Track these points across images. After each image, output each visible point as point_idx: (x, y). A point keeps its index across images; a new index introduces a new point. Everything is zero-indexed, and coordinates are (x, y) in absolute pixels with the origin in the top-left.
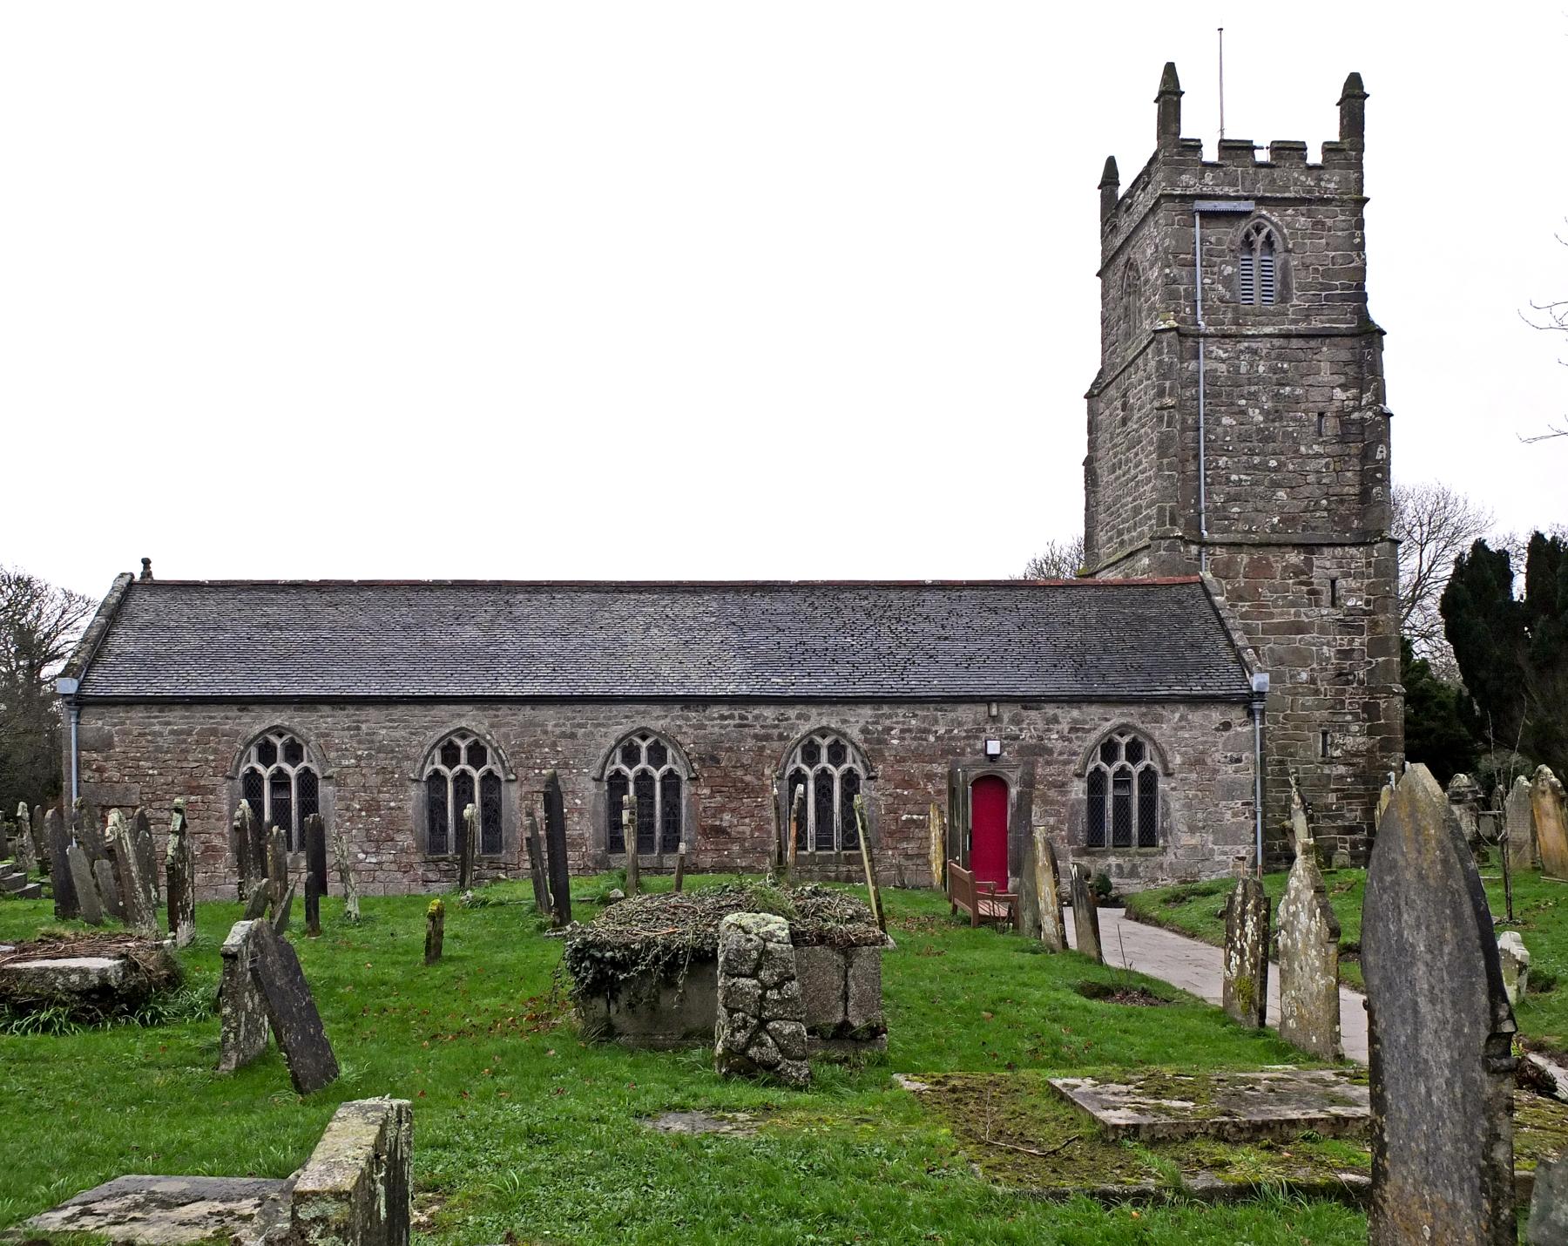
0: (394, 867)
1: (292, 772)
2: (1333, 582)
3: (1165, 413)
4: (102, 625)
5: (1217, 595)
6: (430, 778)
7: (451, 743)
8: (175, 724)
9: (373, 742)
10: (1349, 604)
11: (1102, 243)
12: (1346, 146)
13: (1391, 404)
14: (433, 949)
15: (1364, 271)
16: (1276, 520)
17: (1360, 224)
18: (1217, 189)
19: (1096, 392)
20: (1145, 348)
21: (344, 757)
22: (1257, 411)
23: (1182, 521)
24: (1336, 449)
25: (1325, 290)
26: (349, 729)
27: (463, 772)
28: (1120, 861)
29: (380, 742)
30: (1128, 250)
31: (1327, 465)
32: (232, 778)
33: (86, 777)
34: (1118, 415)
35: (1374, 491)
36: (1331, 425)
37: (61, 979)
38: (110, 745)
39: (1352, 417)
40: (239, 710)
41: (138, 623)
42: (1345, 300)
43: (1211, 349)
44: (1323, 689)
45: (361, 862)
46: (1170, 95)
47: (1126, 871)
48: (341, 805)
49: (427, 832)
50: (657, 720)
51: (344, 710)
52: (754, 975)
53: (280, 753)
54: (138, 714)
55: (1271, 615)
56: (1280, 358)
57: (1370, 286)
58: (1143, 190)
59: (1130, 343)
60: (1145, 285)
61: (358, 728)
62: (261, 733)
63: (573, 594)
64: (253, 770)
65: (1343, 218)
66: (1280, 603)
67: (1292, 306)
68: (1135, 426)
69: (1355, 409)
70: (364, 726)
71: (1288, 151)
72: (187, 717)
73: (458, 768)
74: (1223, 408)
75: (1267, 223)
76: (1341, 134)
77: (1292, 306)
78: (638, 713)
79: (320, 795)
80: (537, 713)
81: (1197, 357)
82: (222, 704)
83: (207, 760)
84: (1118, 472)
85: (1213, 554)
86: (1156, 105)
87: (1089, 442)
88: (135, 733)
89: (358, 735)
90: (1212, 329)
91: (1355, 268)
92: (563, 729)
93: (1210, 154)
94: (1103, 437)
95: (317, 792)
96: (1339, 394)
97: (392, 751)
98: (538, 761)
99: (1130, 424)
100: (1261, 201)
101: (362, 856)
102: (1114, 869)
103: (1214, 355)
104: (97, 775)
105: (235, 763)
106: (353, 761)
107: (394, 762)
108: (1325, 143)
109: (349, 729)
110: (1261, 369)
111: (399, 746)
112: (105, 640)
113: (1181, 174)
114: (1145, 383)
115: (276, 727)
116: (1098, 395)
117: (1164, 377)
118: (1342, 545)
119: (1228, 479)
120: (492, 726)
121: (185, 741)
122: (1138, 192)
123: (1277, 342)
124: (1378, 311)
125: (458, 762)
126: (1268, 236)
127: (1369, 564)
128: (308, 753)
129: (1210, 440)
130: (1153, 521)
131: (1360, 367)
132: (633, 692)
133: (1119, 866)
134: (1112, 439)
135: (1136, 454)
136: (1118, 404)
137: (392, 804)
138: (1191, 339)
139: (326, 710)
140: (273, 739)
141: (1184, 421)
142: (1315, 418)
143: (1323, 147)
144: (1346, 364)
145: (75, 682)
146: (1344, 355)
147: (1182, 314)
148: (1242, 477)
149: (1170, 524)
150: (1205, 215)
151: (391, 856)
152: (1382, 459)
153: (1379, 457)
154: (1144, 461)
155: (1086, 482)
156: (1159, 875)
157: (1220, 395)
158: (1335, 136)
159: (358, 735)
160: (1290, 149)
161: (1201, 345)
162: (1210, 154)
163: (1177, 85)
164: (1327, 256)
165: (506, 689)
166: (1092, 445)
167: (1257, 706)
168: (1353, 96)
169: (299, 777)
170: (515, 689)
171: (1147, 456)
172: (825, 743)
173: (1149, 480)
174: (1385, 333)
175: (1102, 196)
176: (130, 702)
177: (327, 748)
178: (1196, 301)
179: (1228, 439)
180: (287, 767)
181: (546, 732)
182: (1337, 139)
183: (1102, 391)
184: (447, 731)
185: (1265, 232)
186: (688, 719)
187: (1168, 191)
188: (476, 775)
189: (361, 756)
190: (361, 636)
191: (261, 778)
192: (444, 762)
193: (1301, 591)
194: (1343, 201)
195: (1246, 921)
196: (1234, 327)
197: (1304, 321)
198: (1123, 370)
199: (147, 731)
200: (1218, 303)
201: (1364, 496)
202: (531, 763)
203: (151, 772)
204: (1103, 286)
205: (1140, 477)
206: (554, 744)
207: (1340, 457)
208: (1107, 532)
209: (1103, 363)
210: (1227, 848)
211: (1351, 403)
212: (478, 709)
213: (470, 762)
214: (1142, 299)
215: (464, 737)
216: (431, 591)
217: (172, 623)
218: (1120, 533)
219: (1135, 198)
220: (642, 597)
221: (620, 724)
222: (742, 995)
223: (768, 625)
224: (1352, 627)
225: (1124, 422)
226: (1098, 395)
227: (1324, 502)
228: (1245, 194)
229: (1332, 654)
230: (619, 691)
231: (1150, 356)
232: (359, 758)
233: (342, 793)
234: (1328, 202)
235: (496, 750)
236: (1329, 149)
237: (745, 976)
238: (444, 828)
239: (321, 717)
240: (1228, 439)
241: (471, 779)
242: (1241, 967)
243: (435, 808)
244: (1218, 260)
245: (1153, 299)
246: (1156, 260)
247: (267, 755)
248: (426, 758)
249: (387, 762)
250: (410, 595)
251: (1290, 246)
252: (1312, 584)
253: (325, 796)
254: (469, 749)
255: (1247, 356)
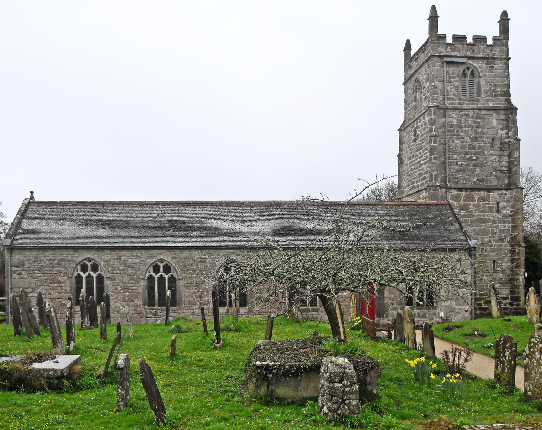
0: (134, 312)
1: (94, 275)
2: (498, 203)
3: (433, 138)
4: (19, 219)
5: (455, 209)
6: (148, 278)
7: (157, 264)
8: (49, 257)
9: (126, 264)
10: (504, 212)
11: (405, 72)
12: (502, 38)
13: (520, 136)
14: (173, 355)
15: (509, 85)
16: (475, 180)
17: (508, 68)
18: (452, 53)
19: (402, 129)
20: (424, 113)
21: (114, 269)
22: (468, 138)
23: (439, 179)
24: (499, 153)
25: (494, 92)
26: (117, 259)
27: (161, 275)
28: (419, 311)
29: (129, 264)
30: (416, 75)
31: (495, 159)
32: (71, 278)
33: (14, 277)
34: (412, 138)
35: (514, 169)
36: (497, 144)
37: (46, 373)
38: (24, 265)
39: (505, 141)
40: (74, 252)
41: (33, 217)
42: (502, 96)
43: (450, 114)
44: (494, 245)
45: (121, 310)
46: (433, 19)
47: (421, 315)
48: (114, 288)
49: (147, 298)
50: (237, 257)
51: (115, 251)
52: (341, 382)
53: (89, 268)
54: (34, 253)
55: (474, 216)
56: (477, 117)
57: (511, 91)
58: (423, 53)
59: (417, 111)
60: (423, 89)
61: (120, 259)
62: (83, 260)
63: (203, 207)
64: (79, 275)
65: (501, 65)
66: (477, 211)
67: (481, 98)
68: (419, 143)
69: (506, 138)
70: (122, 258)
71: (480, 40)
72: (54, 254)
73: (159, 274)
74: (455, 137)
75: (472, 66)
76: (500, 33)
77: (481, 98)
78: (230, 253)
79: (105, 284)
80: (191, 253)
81: (445, 117)
82: (67, 249)
83: (61, 270)
84: (412, 160)
85: (451, 192)
86: (428, 21)
87: (400, 147)
88: (33, 260)
89: (120, 261)
90: (450, 106)
91: (506, 84)
92: (201, 259)
93: (449, 40)
94: (405, 146)
95: (104, 283)
96: (500, 132)
97: (134, 267)
98: (191, 271)
99: (417, 141)
100: (470, 58)
101: (121, 308)
102: (416, 314)
103: (451, 116)
104: (18, 276)
105: (72, 272)
106: (118, 271)
107: (134, 272)
108: (494, 37)
109: (117, 259)
110: (470, 122)
111: (136, 265)
112: (21, 224)
113: (438, 47)
114: (424, 126)
115: (88, 258)
116: (403, 130)
117: (432, 124)
118: (501, 189)
119: (457, 163)
120: (173, 258)
121: (52, 263)
122: (421, 54)
123: (476, 111)
124: (514, 100)
125: (159, 272)
126: (472, 71)
127: (512, 197)
128: (101, 269)
129: (450, 149)
130: (428, 179)
131: (508, 122)
132: (229, 245)
133: (419, 314)
134: (409, 147)
135: (420, 153)
136: (412, 133)
137: (134, 288)
138: (442, 110)
139: (108, 252)
140: (87, 263)
141: (440, 141)
142: (491, 141)
143: (493, 38)
144: (503, 120)
145: (10, 240)
146: (503, 117)
147: (439, 101)
148: (462, 163)
149: (435, 181)
150: (448, 63)
151: (133, 308)
152: (517, 157)
153: (515, 156)
154: (423, 156)
155: (398, 163)
156: (434, 317)
157: (454, 131)
158: (497, 34)
159: (120, 261)
160: (480, 39)
161: (447, 112)
162: (449, 40)
163: (436, 14)
164: (495, 79)
165: (179, 244)
166: (401, 149)
167: (473, 252)
168: (504, 19)
169: (97, 277)
170: (182, 244)
171: (425, 154)
172: (161, 265)
173: (425, 163)
174: (517, 109)
175: (405, 54)
176: (31, 248)
177: (108, 266)
178: (444, 96)
179: (457, 148)
180: (92, 274)
181: (194, 261)
182: (498, 35)
183: (405, 128)
184: (155, 260)
185: (471, 70)
186: (250, 256)
187: (433, 54)
188: (167, 277)
189: (121, 269)
190: (120, 223)
191: (82, 277)
192: (154, 272)
193: (485, 207)
194: (501, 59)
195: (506, 351)
196: (459, 106)
197: (486, 104)
198: (414, 121)
199: (38, 259)
200: (453, 96)
201: (510, 170)
202: (188, 272)
203: (39, 275)
204: (405, 89)
205: (422, 162)
206: (197, 265)
207: (500, 156)
208: (407, 182)
209: (405, 117)
210: (460, 307)
211: (505, 135)
212: (167, 252)
213: (164, 272)
214: (422, 94)
215: (162, 262)
216: (147, 205)
217: (46, 218)
218: (413, 183)
219: (419, 56)
220: (230, 208)
221: (221, 258)
222: (336, 390)
223: (280, 219)
224: (505, 221)
225: (415, 140)
226: (403, 130)
227: (494, 173)
228: (463, 55)
229: (497, 231)
230: (223, 245)
231: (426, 116)
232: (120, 270)
233: (114, 284)
234: (495, 59)
235: (174, 268)
236: (495, 39)
237: (337, 383)
238: (154, 297)
239: (106, 254)
240: (457, 148)
241: (164, 278)
242: (503, 369)
243: (150, 289)
244: (453, 80)
245: (427, 94)
246: (428, 79)
247: (84, 268)
248: (147, 270)
249: (132, 272)
250: (139, 207)
251: (481, 75)
252: (489, 204)
253: (107, 285)
254: (164, 267)
255: (464, 117)
